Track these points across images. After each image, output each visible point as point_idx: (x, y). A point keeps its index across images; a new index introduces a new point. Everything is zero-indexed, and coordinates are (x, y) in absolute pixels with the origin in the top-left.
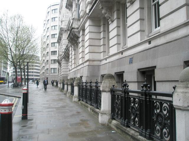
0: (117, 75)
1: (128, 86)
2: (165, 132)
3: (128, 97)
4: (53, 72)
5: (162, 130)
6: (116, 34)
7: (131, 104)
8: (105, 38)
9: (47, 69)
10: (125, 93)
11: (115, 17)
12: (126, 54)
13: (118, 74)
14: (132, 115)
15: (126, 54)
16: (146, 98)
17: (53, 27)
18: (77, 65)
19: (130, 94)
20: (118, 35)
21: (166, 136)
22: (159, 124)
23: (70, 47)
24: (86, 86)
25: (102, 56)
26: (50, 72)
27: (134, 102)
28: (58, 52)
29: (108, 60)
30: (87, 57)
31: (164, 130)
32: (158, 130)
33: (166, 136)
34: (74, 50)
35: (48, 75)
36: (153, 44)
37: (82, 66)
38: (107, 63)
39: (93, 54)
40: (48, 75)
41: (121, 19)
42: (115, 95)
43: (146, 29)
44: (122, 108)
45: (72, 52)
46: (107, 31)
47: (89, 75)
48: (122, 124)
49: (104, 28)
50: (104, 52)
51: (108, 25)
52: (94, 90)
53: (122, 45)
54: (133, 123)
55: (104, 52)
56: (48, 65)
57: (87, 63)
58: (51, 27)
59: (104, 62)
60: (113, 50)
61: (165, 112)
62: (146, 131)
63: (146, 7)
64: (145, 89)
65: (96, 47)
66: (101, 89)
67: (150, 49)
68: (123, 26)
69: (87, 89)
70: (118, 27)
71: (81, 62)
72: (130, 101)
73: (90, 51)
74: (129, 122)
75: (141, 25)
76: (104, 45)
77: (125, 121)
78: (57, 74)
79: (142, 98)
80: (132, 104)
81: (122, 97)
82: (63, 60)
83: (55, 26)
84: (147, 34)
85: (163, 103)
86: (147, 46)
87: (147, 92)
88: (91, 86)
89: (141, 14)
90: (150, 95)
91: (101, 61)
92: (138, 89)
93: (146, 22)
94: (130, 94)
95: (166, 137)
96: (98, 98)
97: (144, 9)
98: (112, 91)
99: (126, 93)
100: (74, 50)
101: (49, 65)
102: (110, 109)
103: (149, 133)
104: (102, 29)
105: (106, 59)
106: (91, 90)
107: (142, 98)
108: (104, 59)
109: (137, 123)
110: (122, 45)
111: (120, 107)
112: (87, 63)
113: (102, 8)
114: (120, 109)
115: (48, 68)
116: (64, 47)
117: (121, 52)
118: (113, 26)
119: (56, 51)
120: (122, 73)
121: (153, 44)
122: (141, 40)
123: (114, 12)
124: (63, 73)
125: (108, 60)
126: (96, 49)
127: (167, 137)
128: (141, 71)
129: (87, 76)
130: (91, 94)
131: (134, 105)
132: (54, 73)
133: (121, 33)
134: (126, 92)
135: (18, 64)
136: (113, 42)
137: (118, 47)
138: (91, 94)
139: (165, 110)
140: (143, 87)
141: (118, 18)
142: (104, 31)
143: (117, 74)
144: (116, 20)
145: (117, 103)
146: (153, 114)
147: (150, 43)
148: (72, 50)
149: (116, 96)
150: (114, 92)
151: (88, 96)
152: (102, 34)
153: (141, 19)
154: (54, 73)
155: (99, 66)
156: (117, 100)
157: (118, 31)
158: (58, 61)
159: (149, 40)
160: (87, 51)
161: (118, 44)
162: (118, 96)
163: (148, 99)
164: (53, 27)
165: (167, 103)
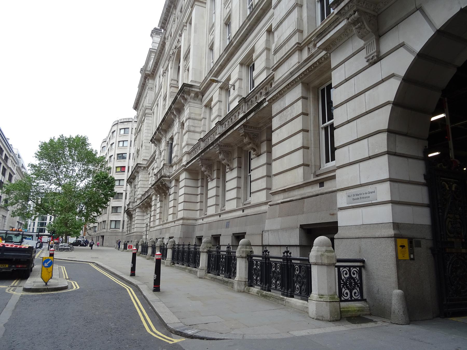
0: (214, 237)
1: (269, 252)
2: (278, 283)
3: (251, 261)
4: (113, 226)
5: (276, 282)
6: (215, 194)
7: (232, 261)
8: (203, 194)
9: (104, 221)
10: (266, 259)
11: (215, 176)
12: (223, 217)
13: (215, 236)
14: (255, 275)
15: (223, 217)
16: (266, 261)
17: (121, 144)
18: (163, 221)
19: (271, 259)
20: (217, 196)
21: (279, 286)
22: (299, 283)
23: (153, 195)
24: (183, 248)
25: (197, 215)
26: (109, 227)
27: (257, 265)
28: (124, 194)
29: (206, 220)
30: (180, 215)
31: (278, 282)
32: (274, 283)
33: (279, 286)
34: (160, 201)
35: (104, 230)
36: (247, 212)
37: (173, 224)
38: (204, 224)
39: (188, 211)
40: (104, 230)
41: (221, 179)
42: (220, 256)
43: (242, 196)
44: (215, 264)
45: (156, 203)
46: (205, 186)
47: (182, 236)
48: (262, 289)
49: (202, 183)
50: (201, 210)
51: (207, 182)
52: (192, 251)
53: (220, 206)
54: (274, 287)
55: (201, 210)
56: (106, 215)
57: (181, 222)
58: (117, 142)
59: (200, 222)
60: (211, 211)
61: (259, 267)
62: (287, 291)
63: (243, 176)
64: (285, 254)
65: (192, 204)
66: (201, 250)
67: (257, 214)
68: (222, 187)
69: (197, 252)
70: (217, 187)
71: (170, 218)
72: (232, 258)
73: (185, 209)
74: (293, 291)
75: (238, 193)
76: (201, 202)
77: (265, 286)
78: (121, 230)
79: (284, 263)
80: (255, 267)
81: (281, 265)
82: (137, 210)
83: (123, 141)
84: (242, 202)
85: (295, 265)
86: (240, 213)
87: (288, 257)
88: (183, 248)
89: (238, 182)
90: (269, 258)
91: (196, 220)
92: (300, 257)
93: (242, 190)
94: (271, 259)
95: (297, 291)
96: (231, 265)
97: (241, 178)
98: (209, 252)
99: (267, 259)
100: (161, 201)
101: (109, 215)
102: (247, 277)
103: (290, 292)
104: (200, 184)
105: (203, 219)
106: (183, 252)
107: (284, 263)
108: (200, 219)
109: (304, 291)
110: (220, 206)
111: (224, 264)
112: (181, 222)
113: (220, 153)
114: (224, 266)
115: (105, 219)
116: (140, 192)
117: (220, 214)
118: (212, 184)
119: (122, 194)
120: (219, 236)
121: (247, 212)
122: (237, 207)
123: (214, 171)
124: (135, 230)
125: (206, 220)
126: (191, 206)
127: (279, 287)
128: (235, 235)
129: (180, 238)
130: (183, 255)
131: (276, 269)
132: (115, 228)
133: (220, 194)
134: (218, 252)
135: (84, 177)
136: (211, 202)
137: (173, 209)
138: (183, 255)
139: (278, 268)
140: (284, 253)
141: (218, 178)
142: (202, 186)
143: (214, 236)
144: (216, 179)
145: (191, 256)
146: (294, 275)
147: (243, 211)
148: (156, 200)
149: (221, 256)
150: (210, 252)
151: (175, 257)
152: (199, 189)
153: (238, 188)
154: (115, 228)
155: (194, 225)
156: (233, 261)
157: (217, 191)
158: (129, 211)
159: (243, 209)
160: (181, 207)
161: (217, 205)
162: (223, 256)
163: (267, 262)
164: (120, 142)
165: (298, 265)
